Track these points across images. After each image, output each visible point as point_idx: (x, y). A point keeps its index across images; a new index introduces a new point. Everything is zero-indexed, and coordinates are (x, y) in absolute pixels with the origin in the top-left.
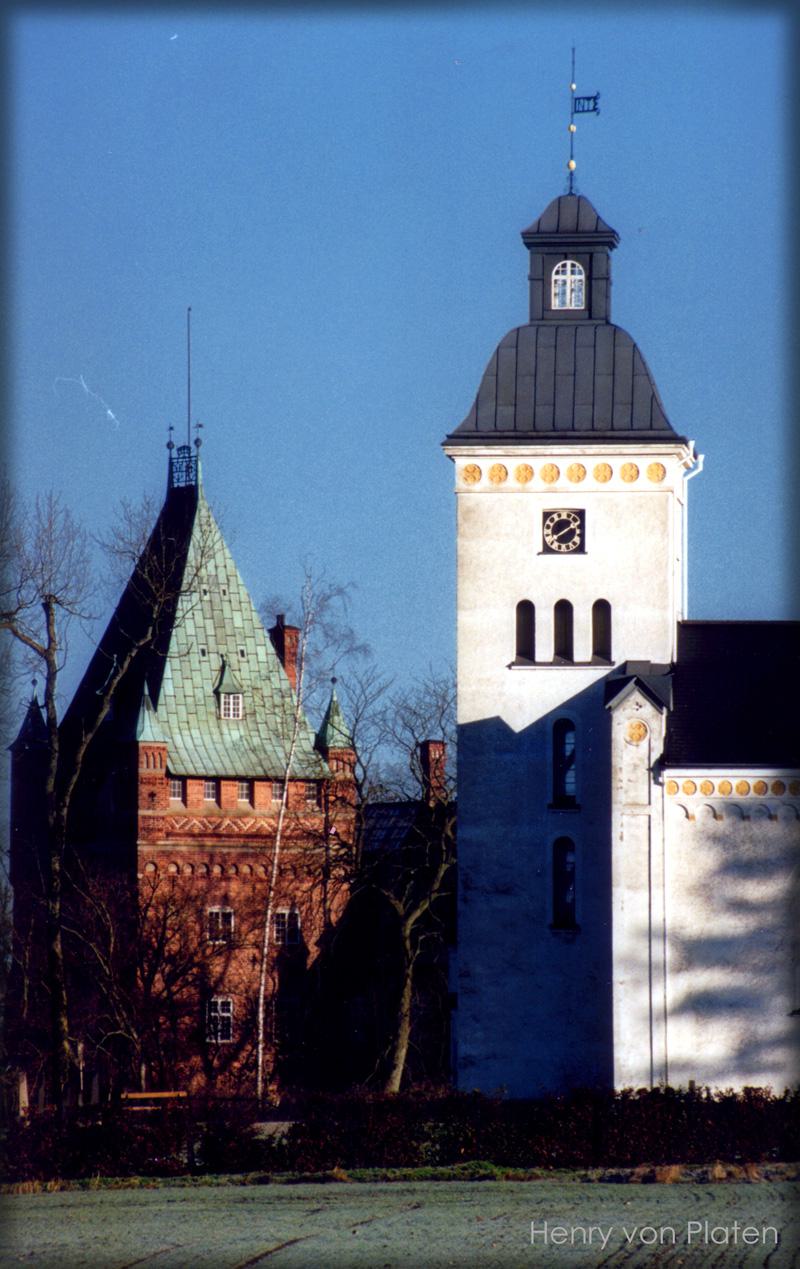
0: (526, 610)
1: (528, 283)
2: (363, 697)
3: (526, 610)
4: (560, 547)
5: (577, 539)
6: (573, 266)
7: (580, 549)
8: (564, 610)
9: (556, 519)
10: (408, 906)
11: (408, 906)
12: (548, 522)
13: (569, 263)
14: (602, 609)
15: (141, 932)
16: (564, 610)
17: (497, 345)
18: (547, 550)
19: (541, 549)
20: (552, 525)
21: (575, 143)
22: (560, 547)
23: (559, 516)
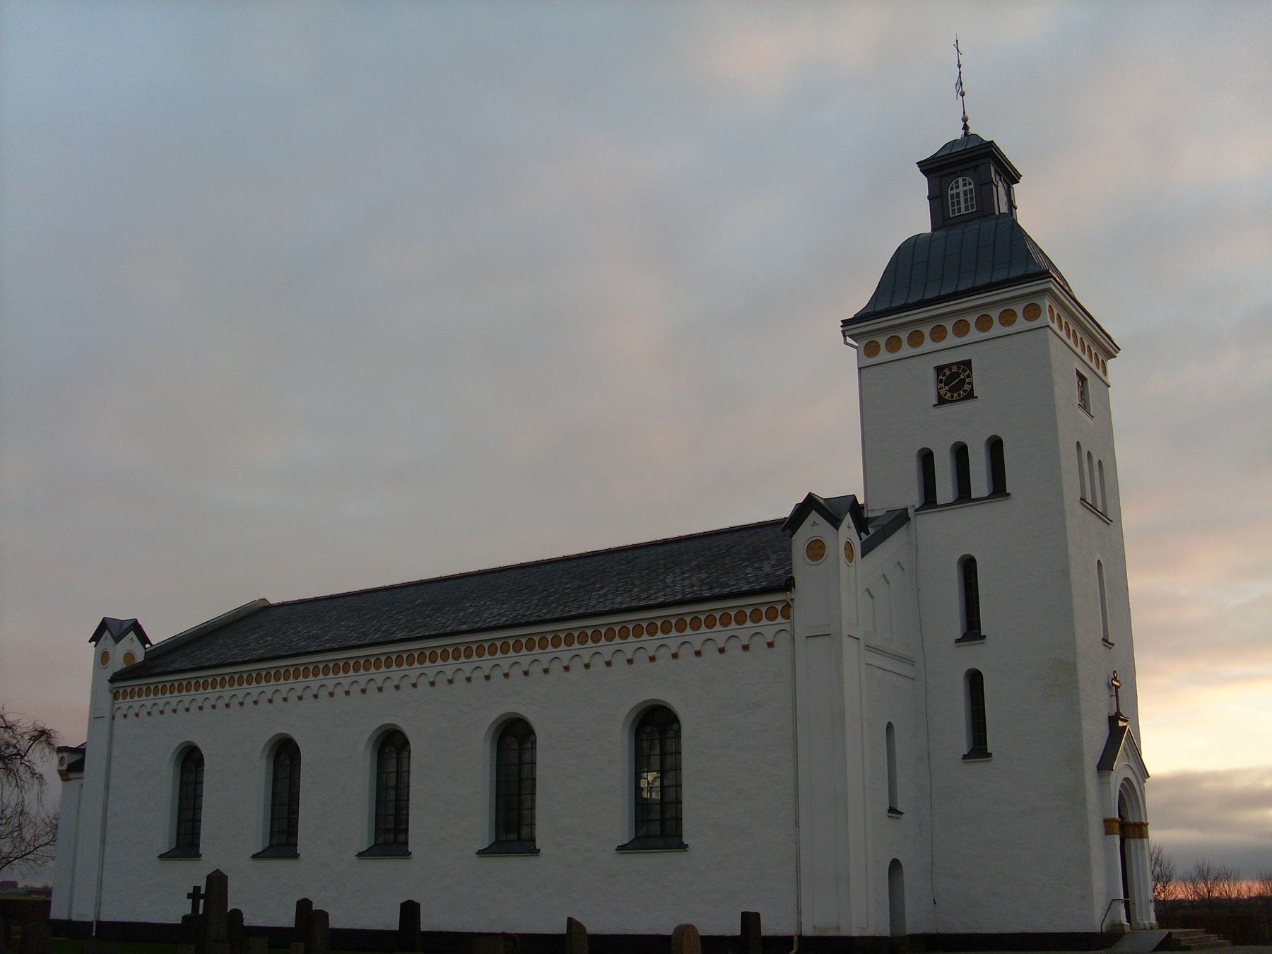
0: (926, 459)
1: (928, 201)
2: (12, 859)
3: (926, 459)
4: (952, 396)
5: (967, 387)
6: (964, 180)
7: (970, 396)
8: (960, 452)
9: (948, 373)
10: (1069, 463)
11: (1069, 463)
12: (941, 377)
13: (960, 179)
14: (995, 447)
15: (645, 772)
16: (960, 452)
17: (1082, 448)
18: (942, 401)
19: (935, 402)
20: (944, 378)
21: (1000, 205)
22: (952, 396)
23: (950, 370)
